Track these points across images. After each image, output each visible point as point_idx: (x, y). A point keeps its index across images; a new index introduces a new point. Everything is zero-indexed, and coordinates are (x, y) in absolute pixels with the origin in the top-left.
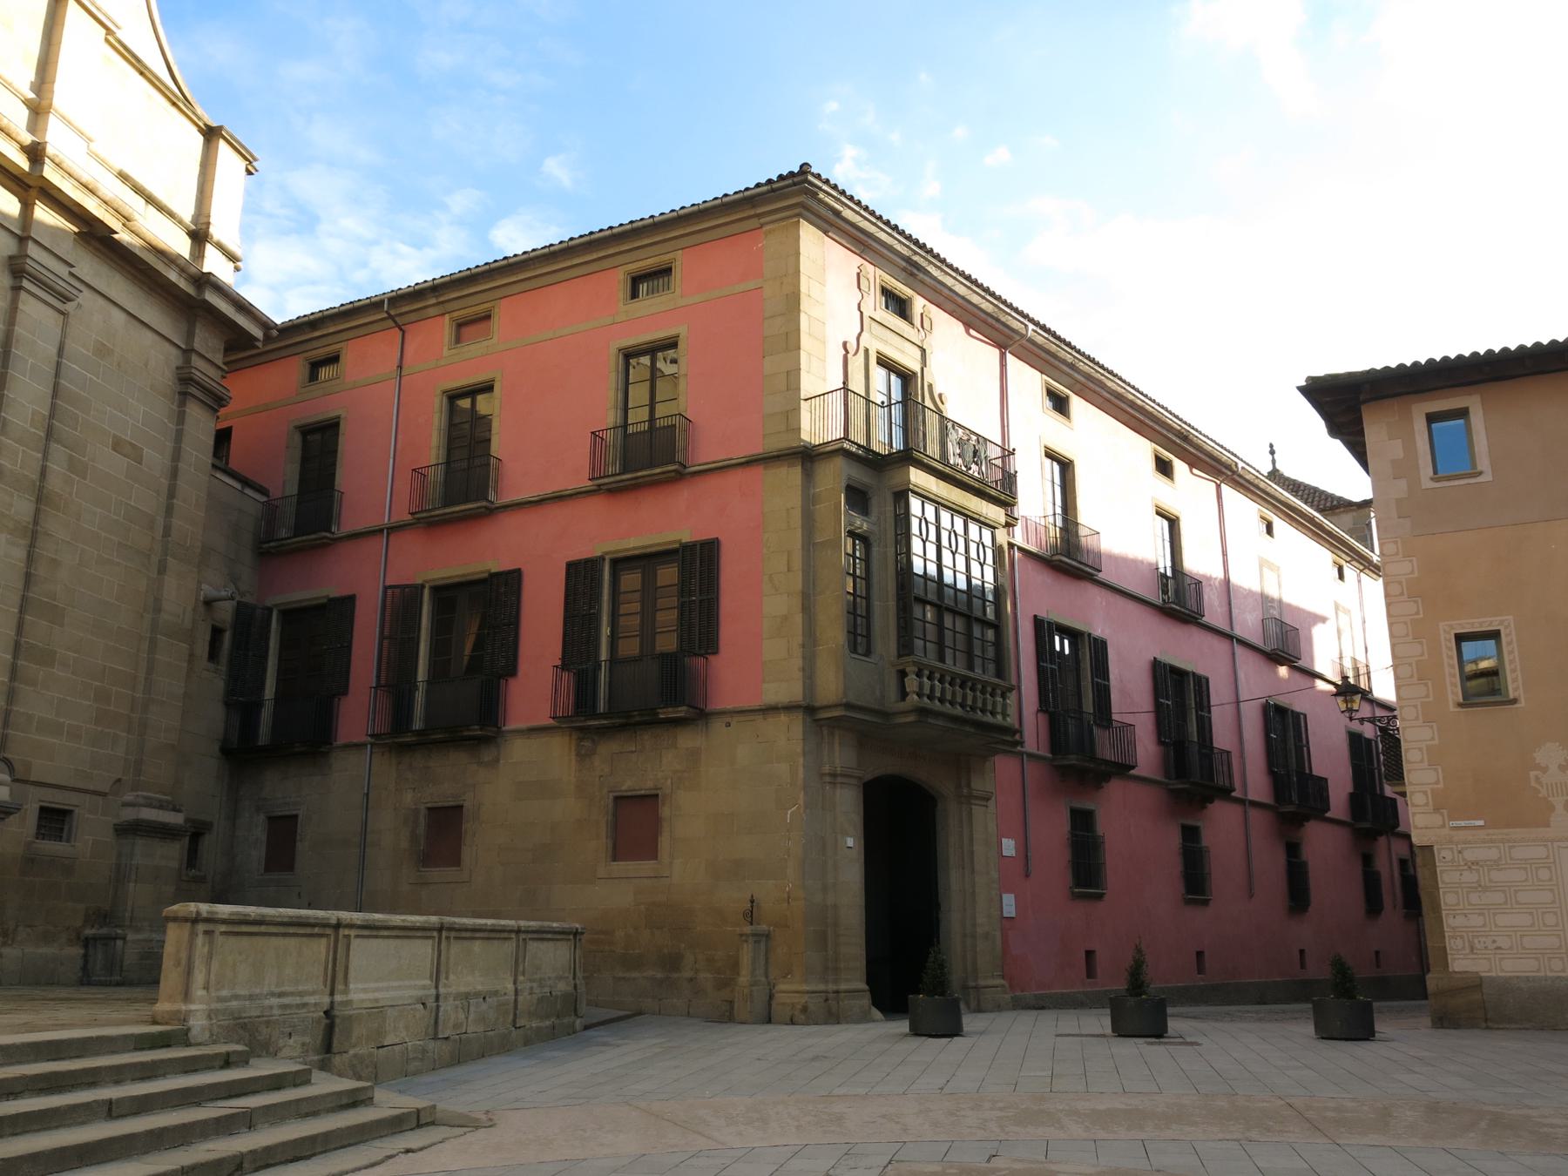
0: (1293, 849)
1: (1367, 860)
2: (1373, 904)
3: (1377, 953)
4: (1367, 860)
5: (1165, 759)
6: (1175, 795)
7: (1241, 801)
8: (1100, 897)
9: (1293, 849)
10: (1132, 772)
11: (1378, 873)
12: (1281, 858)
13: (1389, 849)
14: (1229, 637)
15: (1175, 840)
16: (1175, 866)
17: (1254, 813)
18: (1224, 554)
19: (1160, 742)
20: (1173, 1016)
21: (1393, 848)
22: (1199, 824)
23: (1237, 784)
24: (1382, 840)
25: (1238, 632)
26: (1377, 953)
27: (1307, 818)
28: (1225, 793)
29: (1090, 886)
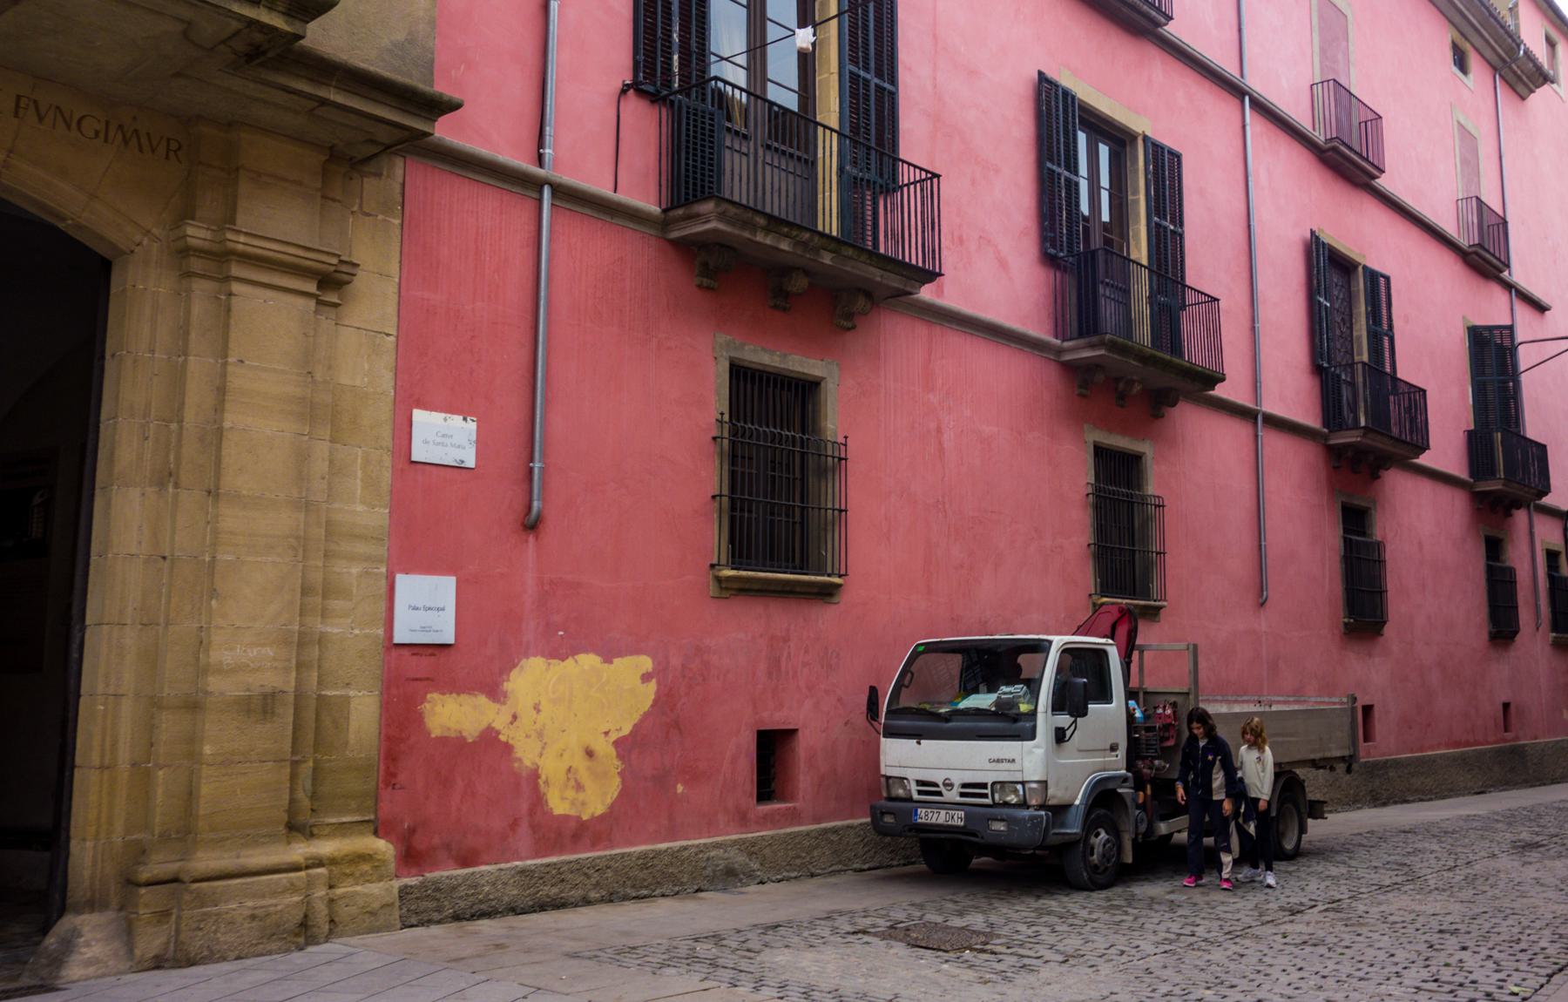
0: (1355, 520)
1: (1494, 548)
2: (1503, 628)
3: (1506, 706)
4: (1494, 548)
5: (1058, 297)
6: (1080, 377)
7: (1246, 414)
8: (826, 593)
9: (1355, 520)
10: (926, 293)
11: (1511, 572)
12: (1333, 535)
13: (1531, 534)
14: (1236, 91)
15: (1080, 475)
16: (1074, 531)
17: (1276, 445)
18: (1240, 30)
19: (1049, 259)
20: (1141, 681)
21: (1538, 529)
22: (1144, 447)
23: (1234, 364)
24: (1520, 517)
25: (1255, 82)
26: (1506, 706)
27: (1517, 504)
28: (1200, 383)
29: (803, 568)
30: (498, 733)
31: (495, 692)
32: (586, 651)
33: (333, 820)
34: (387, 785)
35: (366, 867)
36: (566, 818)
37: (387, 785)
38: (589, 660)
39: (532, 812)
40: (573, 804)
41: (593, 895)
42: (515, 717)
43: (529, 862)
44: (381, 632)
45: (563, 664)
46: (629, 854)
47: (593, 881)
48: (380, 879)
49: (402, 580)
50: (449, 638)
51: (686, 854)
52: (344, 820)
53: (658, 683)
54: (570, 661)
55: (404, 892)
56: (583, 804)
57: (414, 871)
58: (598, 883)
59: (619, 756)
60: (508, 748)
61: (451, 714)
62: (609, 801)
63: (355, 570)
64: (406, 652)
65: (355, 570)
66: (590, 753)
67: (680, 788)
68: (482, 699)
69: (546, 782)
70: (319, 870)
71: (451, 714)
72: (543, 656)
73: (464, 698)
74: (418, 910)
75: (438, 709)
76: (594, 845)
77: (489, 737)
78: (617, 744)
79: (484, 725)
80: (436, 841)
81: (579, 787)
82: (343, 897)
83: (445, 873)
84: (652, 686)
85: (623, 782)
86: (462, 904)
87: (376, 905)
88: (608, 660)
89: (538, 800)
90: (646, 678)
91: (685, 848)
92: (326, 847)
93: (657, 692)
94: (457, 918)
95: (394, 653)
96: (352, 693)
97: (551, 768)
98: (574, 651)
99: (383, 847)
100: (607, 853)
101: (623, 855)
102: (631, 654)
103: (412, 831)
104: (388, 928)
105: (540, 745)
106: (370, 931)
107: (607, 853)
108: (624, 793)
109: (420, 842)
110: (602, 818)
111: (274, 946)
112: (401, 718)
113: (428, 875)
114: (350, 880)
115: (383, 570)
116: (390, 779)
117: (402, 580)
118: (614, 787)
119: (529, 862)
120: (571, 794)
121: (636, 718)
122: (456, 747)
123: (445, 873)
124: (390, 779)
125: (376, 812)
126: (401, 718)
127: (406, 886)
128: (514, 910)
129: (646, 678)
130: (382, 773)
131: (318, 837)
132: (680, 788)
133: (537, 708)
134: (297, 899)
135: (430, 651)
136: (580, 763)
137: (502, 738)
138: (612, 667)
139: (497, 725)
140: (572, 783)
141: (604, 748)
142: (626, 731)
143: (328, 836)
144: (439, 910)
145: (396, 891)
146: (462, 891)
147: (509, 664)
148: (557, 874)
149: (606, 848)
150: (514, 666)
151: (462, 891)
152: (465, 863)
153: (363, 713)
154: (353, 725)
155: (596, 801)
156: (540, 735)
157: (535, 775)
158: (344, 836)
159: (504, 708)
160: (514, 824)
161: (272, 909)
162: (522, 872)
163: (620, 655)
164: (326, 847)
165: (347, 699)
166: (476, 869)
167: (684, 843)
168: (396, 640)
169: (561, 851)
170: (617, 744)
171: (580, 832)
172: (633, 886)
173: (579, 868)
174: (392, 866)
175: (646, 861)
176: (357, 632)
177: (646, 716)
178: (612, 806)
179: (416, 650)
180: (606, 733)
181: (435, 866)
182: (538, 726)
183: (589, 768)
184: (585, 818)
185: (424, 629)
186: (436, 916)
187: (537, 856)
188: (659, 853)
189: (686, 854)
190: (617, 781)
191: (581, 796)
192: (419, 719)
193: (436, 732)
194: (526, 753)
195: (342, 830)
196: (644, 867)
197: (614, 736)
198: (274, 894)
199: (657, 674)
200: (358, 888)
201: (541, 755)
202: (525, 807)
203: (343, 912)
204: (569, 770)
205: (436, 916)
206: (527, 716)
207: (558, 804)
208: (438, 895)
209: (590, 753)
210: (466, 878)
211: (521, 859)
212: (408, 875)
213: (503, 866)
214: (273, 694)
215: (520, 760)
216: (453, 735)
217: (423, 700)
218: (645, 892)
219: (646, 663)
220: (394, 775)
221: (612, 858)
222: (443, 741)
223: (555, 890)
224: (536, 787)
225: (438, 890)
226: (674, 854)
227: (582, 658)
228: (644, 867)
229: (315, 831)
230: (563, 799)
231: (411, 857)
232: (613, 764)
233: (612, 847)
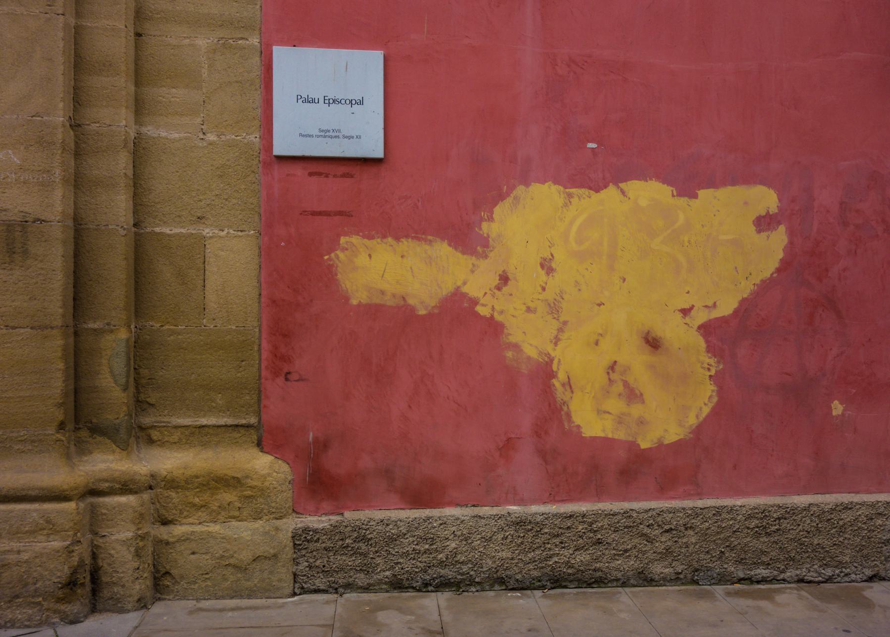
30: (474, 302)
31: (466, 237)
32: (642, 176)
33: (187, 421)
34: (276, 373)
35: (228, 496)
36: (607, 443)
37: (276, 373)
38: (648, 192)
39: (540, 431)
40: (620, 420)
41: (659, 569)
42: (504, 279)
43: (535, 508)
44: (254, 138)
45: (595, 196)
46: (731, 510)
47: (660, 547)
48: (257, 517)
49: (282, 55)
50: (372, 145)
51: (847, 516)
52: (204, 421)
53: (791, 233)
54: (611, 192)
55: (302, 540)
56: (641, 422)
57: (326, 506)
58: (668, 551)
59: (711, 349)
60: (494, 328)
61: (383, 269)
62: (692, 421)
63: (202, 42)
64: (299, 171)
65: (202, 42)
66: (653, 343)
67: (837, 408)
68: (443, 249)
69: (568, 384)
70: (123, 499)
71: (383, 269)
72: (556, 182)
73: (406, 244)
74: (318, 567)
75: (362, 260)
76: (664, 489)
77: (457, 309)
78: (706, 329)
79: (448, 288)
80: (366, 462)
81: (632, 395)
82: (185, 539)
83: (379, 515)
84: (779, 238)
85: (721, 391)
86: (408, 565)
87: (245, 556)
88: (680, 195)
89: (552, 412)
90: (765, 223)
91: (847, 507)
92: (168, 461)
93: (790, 248)
94: (397, 585)
95: (278, 171)
96: (207, 232)
97: (575, 361)
98: (618, 176)
99: (261, 464)
100: (688, 503)
101: (718, 511)
102: (734, 183)
103: (322, 445)
104: (268, 591)
105: (555, 324)
106: (236, 594)
107: (688, 503)
108: (722, 409)
109: (336, 462)
110: (678, 446)
111: (19, 614)
112: (296, 280)
113: (348, 514)
114: (203, 515)
115: (255, 41)
116: (280, 364)
117: (282, 55)
118: (702, 400)
119: (535, 508)
120: (615, 405)
121: (746, 289)
122: (395, 323)
123: (379, 515)
124: (280, 364)
125: (259, 414)
126: (296, 280)
127: (306, 530)
128: (502, 582)
129: (765, 223)
130: (265, 355)
131: (162, 444)
132: (837, 408)
133: (547, 266)
134: (57, 544)
135: (342, 169)
136: (637, 361)
137: (482, 310)
138: (695, 203)
139: (472, 290)
140: (619, 388)
141: (681, 335)
142: (727, 307)
143: (177, 444)
144: (367, 569)
145: (285, 537)
146: (407, 544)
147: (494, 195)
148: (591, 532)
149: (687, 496)
150: (501, 197)
151: (407, 544)
152: (417, 500)
153: (229, 265)
154: (214, 280)
155: (668, 418)
156: (554, 309)
157: (545, 372)
158: (205, 445)
159: (483, 264)
160: (508, 447)
161: (12, 557)
162: (520, 523)
163: (712, 184)
164: (168, 461)
165: (202, 240)
166: (435, 512)
167: (846, 498)
168: (278, 150)
169: (600, 494)
170: (706, 329)
171: (634, 467)
172: (740, 561)
173: (630, 524)
174: (285, 497)
175: (765, 523)
176: (211, 137)
177: (766, 286)
178: (698, 430)
179: (314, 167)
180: (685, 312)
181: (363, 500)
182: (549, 295)
183: (651, 367)
184: (644, 445)
185: (325, 134)
186: (361, 579)
187: (552, 498)
188: (793, 511)
189: (847, 516)
190: (710, 389)
191: (636, 410)
192: (329, 276)
193: (359, 297)
194: (529, 337)
195: (199, 436)
196: (762, 531)
197: (701, 317)
198: (15, 534)
199: (790, 215)
200: (215, 528)
201: (556, 341)
202: (526, 423)
203: (184, 562)
204: (612, 367)
205: (361, 579)
206: (528, 280)
207: (591, 418)
208: (363, 547)
209: (653, 343)
210: (413, 526)
211: (521, 502)
212: (316, 512)
213: (486, 511)
214: (24, 224)
215: (516, 347)
216: (390, 302)
217: (334, 245)
218: (762, 572)
219: (766, 199)
220: (286, 359)
221: (696, 513)
222: (373, 311)
223: (583, 557)
224: (547, 391)
225: (364, 539)
226: (825, 516)
227: (634, 187)
228: (762, 531)
229: (155, 435)
230: (600, 412)
231: (320, 483)
232: (701, 363)
233: (700, 495)
